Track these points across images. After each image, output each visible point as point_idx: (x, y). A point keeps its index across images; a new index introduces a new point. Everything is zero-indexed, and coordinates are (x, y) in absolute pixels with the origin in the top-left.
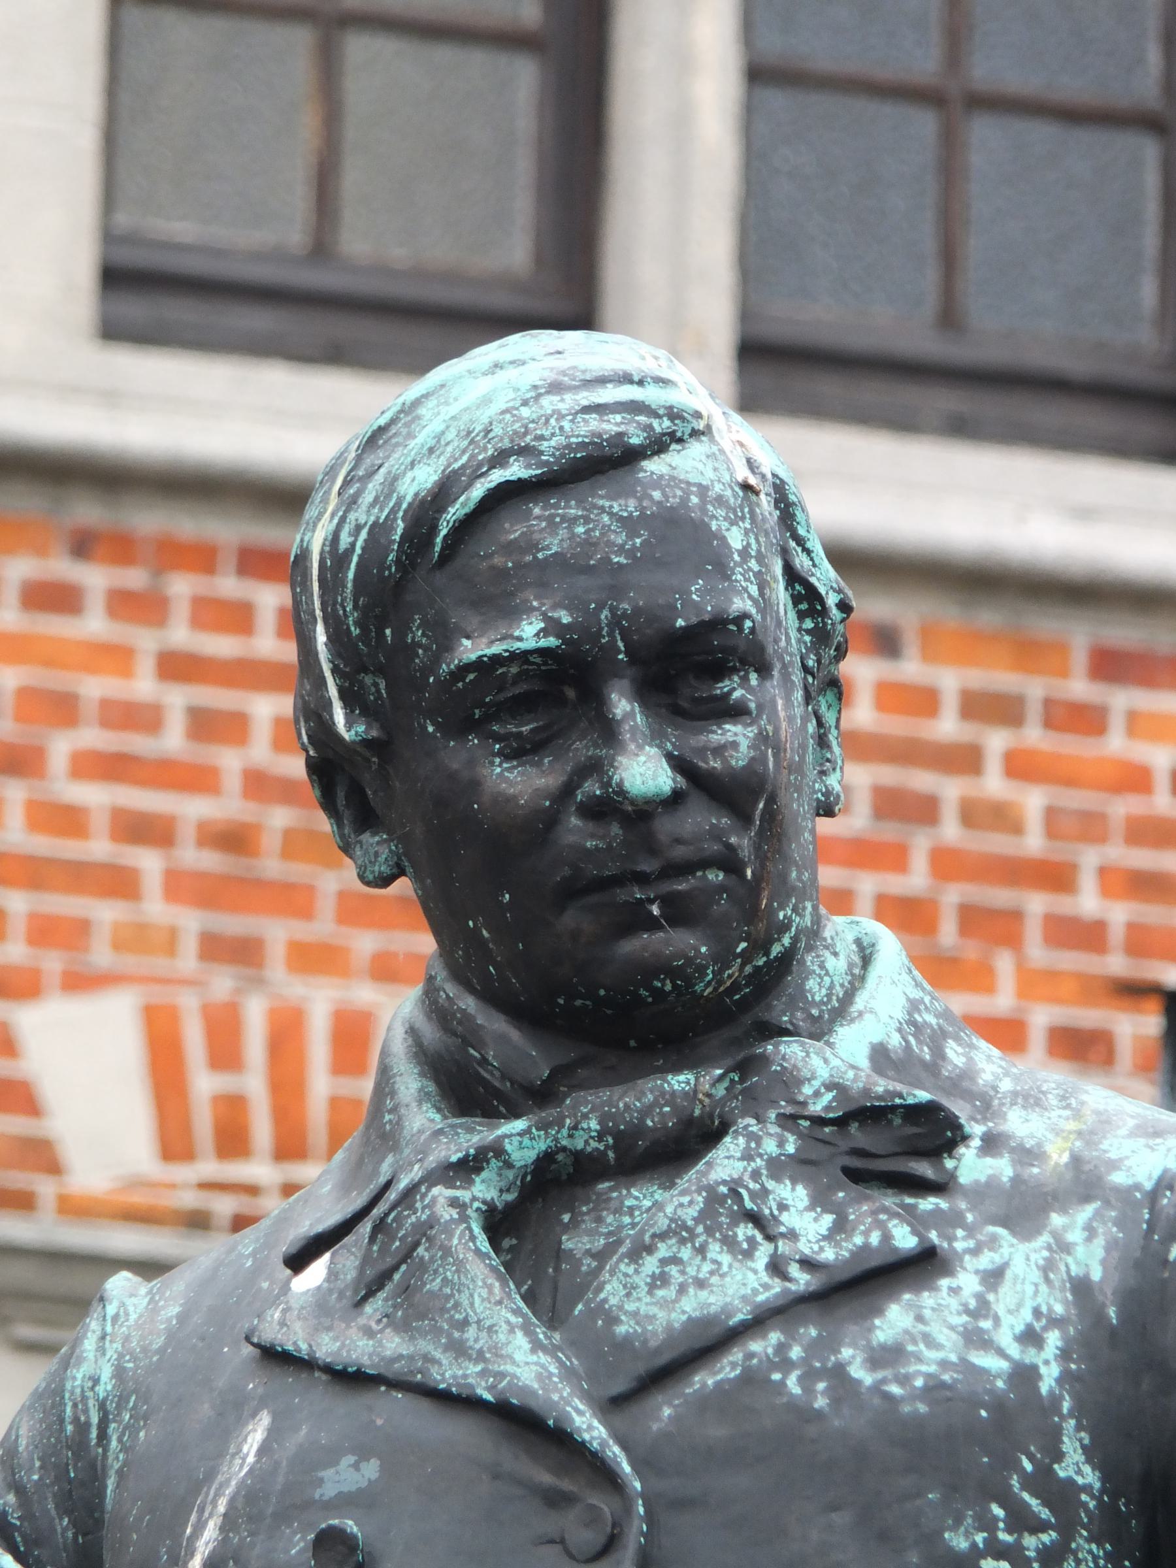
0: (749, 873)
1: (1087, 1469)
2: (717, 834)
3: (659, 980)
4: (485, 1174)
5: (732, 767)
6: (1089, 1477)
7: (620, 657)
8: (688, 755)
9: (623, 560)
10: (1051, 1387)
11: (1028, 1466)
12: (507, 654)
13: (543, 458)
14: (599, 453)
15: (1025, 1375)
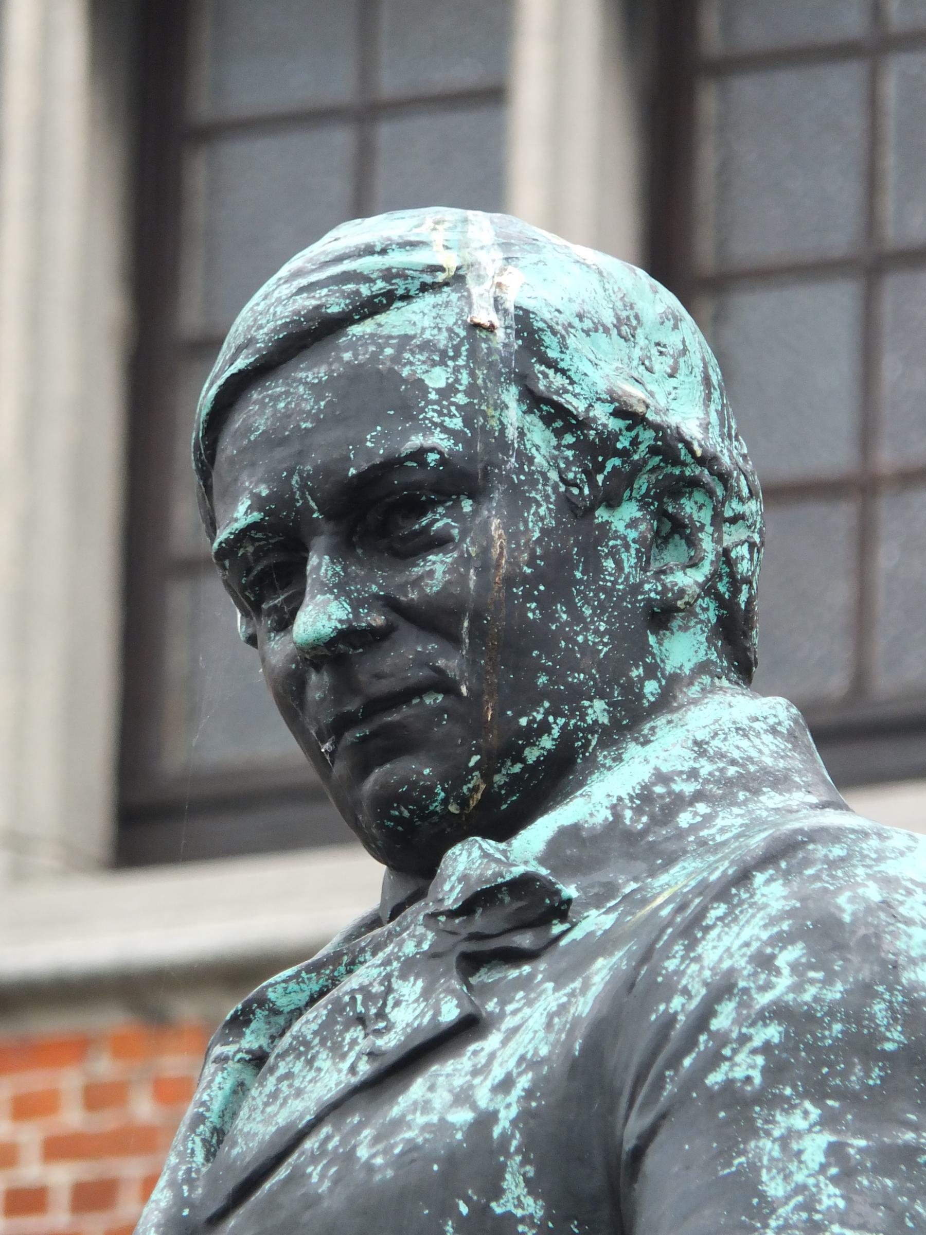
1: (529, 1201)
2: (422, 661)
3: (394, 809)
4: (253, 1025)
5: (427, 595)
6: (533, 1207)
7: (315, 515)
8: (392, 592)
9: (309, 425)
10: (504, 1128)
11: (464, 1209)
12: (232, 537)
13: (258, 345)
14: (298, 330)
15: (486, 1119)
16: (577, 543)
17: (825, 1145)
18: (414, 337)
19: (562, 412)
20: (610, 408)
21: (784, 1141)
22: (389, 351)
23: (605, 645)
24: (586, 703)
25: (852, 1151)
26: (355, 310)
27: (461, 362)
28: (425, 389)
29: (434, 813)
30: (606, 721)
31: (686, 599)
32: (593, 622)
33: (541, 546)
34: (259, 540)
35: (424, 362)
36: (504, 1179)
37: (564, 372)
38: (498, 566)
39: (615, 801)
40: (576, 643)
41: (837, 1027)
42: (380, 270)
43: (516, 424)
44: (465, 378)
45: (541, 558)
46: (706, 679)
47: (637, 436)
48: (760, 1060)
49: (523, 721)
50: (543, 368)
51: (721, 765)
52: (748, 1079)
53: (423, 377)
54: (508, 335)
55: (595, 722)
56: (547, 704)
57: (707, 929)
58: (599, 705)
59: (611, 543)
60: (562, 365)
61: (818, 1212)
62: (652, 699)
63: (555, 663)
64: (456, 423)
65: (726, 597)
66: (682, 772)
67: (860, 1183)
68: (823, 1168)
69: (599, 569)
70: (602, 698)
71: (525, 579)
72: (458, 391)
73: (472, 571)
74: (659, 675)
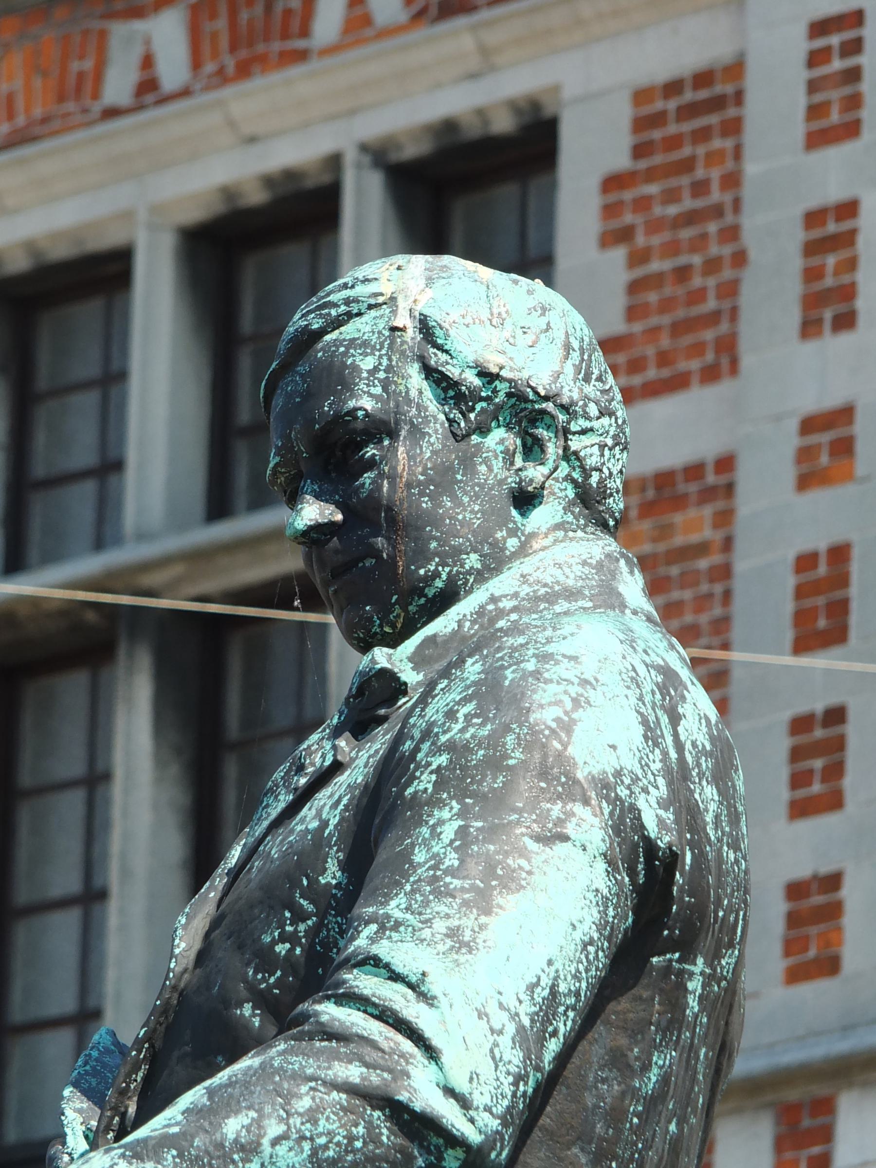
0: (385, 555)
16: (457, 457)
17: (456, 828)
18: (358, 339)
19: (444, 377)
20: (475, 371)
21: (433, 828)
22: (342, 349)
23: (479, 519)
24: (465, 556)
25: (472, 830)
26: (328, 325)
27: (384, 352)
28: (360, 370)
29: (376, 633)
30: (479, 567)
31: (534, 485)
32: (469, 505)
33: (431, 461)
34: (285, 473)
35: (361, 354)
36: (327, 862)
37: (447, 352)
38: (401, 477)
39: (461, 617)
40: (458, 520)
41: (481, 752)
42: (344, 299)
43: (417, 387)
44: (385, 362)
45: (431, 469)
46: (560, 534)
47: (496, 387)
48: (434, 777)
49: (422, 572)
50: (435, 350)
51: (536, 588)
52: (426, 789)
53: (360, 363)
54: (415, 332)
55: (472, 568)
56: (437, 560)
57: (433, 698)
58: (474, 557)
59: (484, 455)
60: (446, 347)
61: (440, 870)
62: (513, 550)
63: (442, 534)
64: (378, 390)
65: (580, 480)
66: (508, 595)
67: (472, 849)
68: (452, 842)
69: (475, 472)
70: (475, 552)
71: (419, 483)
72: (380, 370)
73: (385, 482)
74: (519, 534)
